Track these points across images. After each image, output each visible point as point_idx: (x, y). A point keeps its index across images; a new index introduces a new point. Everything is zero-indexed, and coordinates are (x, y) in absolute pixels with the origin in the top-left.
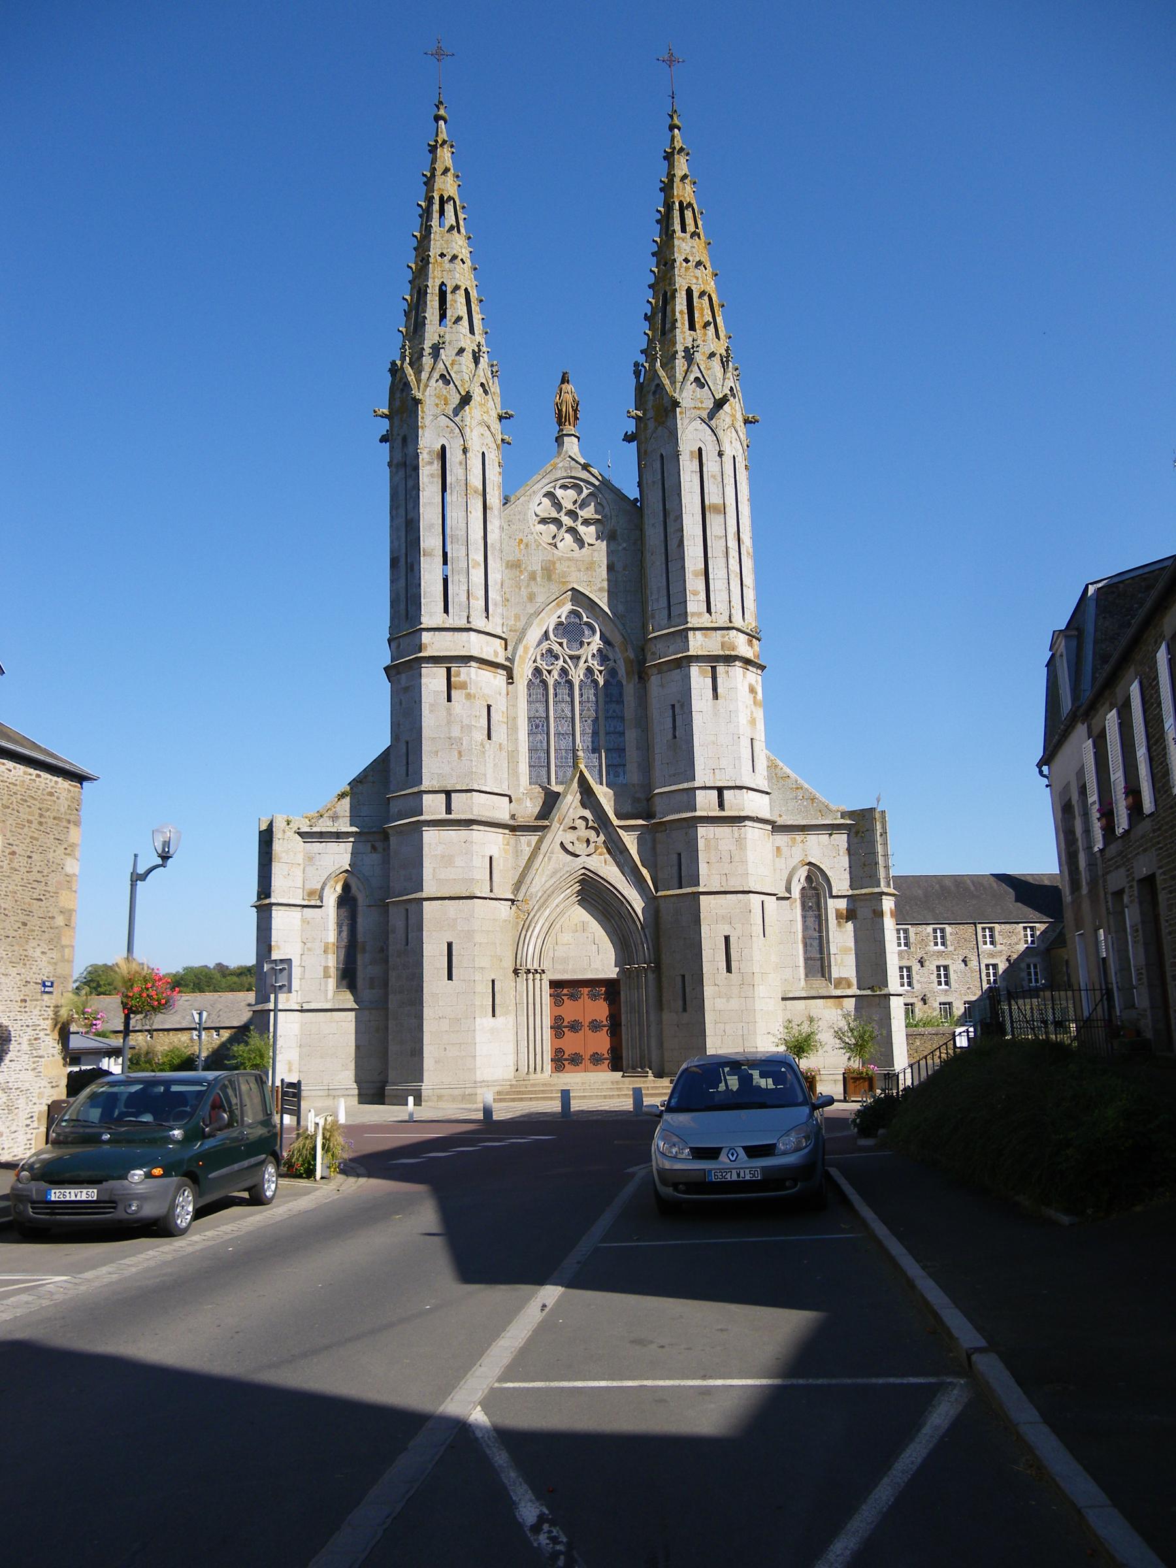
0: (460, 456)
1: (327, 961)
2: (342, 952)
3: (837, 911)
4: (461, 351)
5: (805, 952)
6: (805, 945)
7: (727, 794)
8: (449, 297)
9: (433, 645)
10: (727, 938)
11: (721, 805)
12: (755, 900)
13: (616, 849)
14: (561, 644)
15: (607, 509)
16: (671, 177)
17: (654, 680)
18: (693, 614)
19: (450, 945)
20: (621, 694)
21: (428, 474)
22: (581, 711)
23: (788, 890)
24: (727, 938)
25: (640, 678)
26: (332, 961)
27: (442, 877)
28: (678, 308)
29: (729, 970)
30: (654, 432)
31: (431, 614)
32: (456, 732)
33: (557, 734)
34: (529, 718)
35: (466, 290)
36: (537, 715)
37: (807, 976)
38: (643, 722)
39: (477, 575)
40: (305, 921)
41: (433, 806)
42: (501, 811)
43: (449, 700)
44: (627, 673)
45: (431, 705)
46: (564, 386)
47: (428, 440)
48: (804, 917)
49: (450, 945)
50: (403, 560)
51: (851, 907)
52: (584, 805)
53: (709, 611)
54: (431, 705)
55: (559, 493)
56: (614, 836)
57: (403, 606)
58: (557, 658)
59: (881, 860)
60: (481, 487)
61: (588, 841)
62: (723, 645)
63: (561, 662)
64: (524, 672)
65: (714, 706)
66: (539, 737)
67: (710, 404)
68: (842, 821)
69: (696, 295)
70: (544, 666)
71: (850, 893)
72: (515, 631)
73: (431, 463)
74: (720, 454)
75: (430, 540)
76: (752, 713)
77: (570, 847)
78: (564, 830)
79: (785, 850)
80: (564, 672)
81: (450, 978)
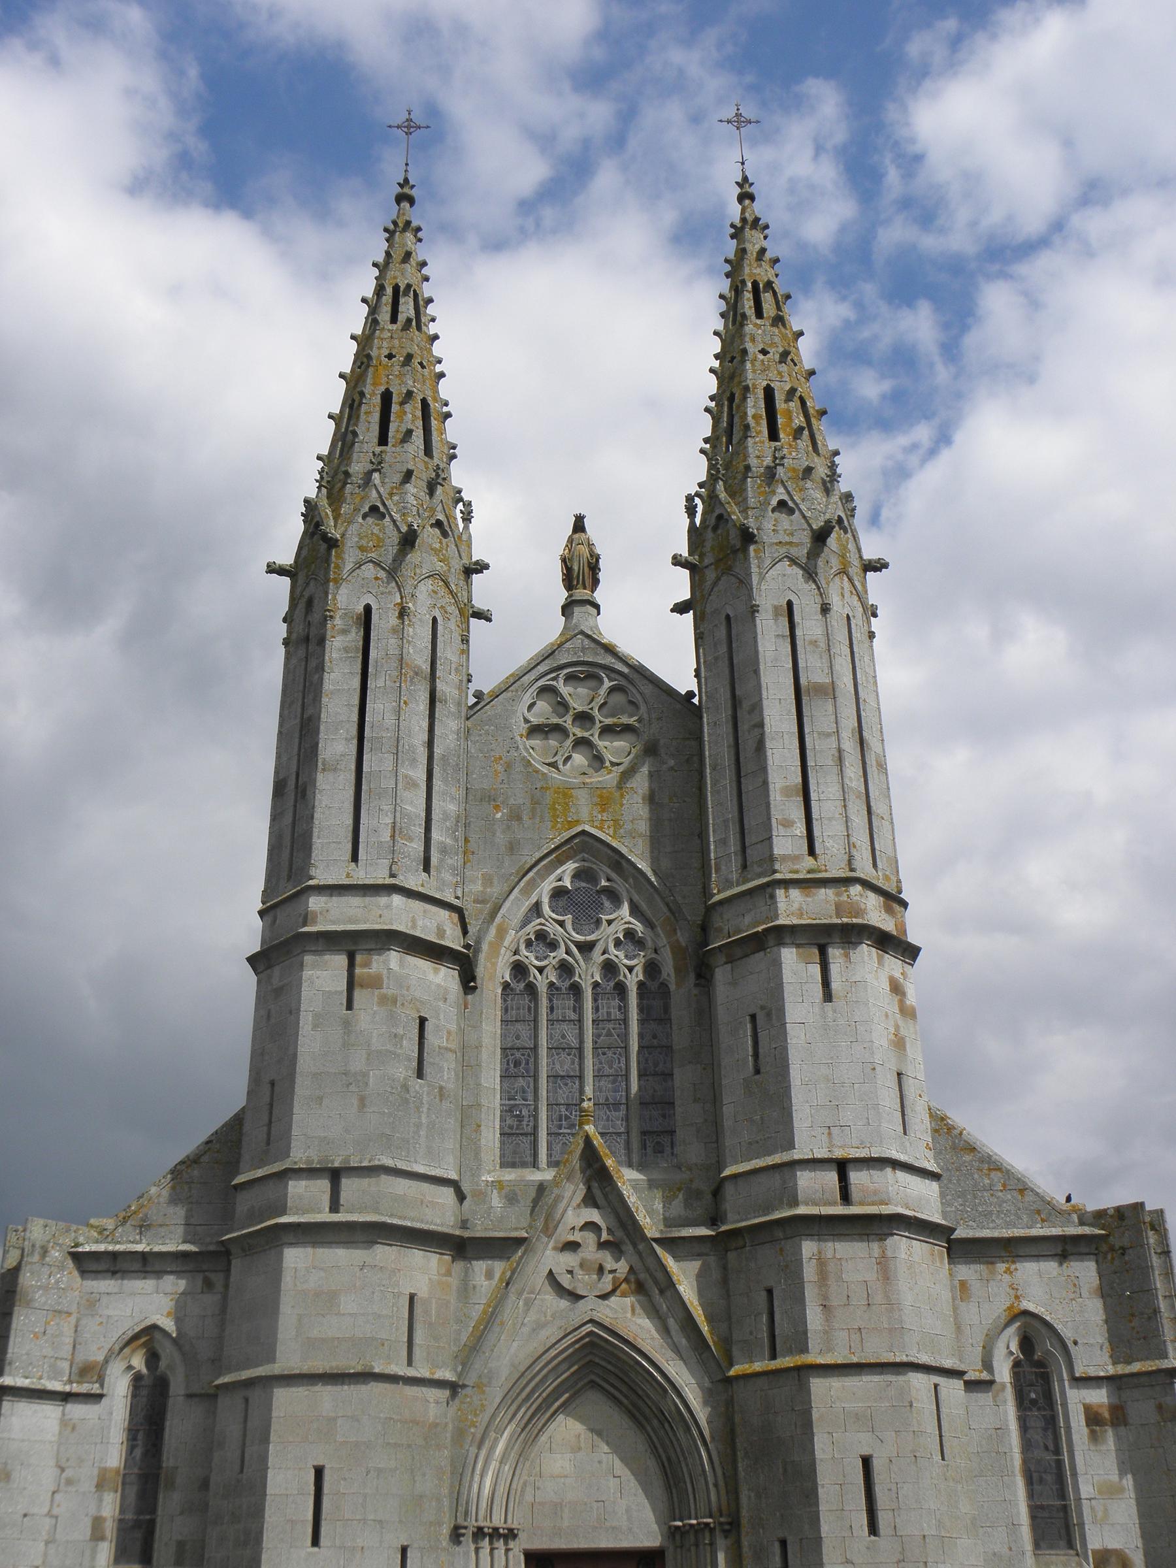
0: (393, 621)
1: (99, 1507)
2: (132, 1492)
3: (1088, 1409)
4: (408, 475)
5: (1031, 1495)
6: (1029, 1481)
7: (856, 1177)
8: (395, 408)
9: (330, 914)
10: (866, 1462)
11: (846, 1197)
12: (920, 1383)
13: (651, 1286)
14: (561, 924)
15: (643, 709)
16: (742, 252)
17: (721, 975)
18: (785, 858)
19: (319, 1472)
20: (666, 1009)
21: (340, 645)
22: (596, 1036)
23: (988, 1365)
24: (866, 1462)
25: (699, 976)
26: (110, 1506)
27: (315, 1333)
28: (750, 412)
29: (873, 1529)
30: (715, 584)
31: (328, 863)
32: (358, 1063)
33: (553, 1077)
34: (503, 1049)
35: (424, 402)
36: (518, 1043)
37: (1037, 1545)
38: (706, 1051)
39: (415, 804)
40: (65, 1423)
41: (307, 1200)
42: (438, 1211)
43: (350, 1006)
44: (678, 970)
45: (317, 1016)
46: (576, 536)
47: (346, 599)
48: (1024, 1427)
49: (319, 1472)
50: (291, 783)
51: (1116, 1401)
52: (589, 1200)
53: (812, 852)
54: (317, 1016)
55: (565, 690)
56: (650, 1261)
57: (286, 854)
58: (553, 946)
59: (1156, 1261)
60: (426, 667)
61: (601, 1270)
62: (839, 909)
63: (561, 953)
64: (494, 970)
65: (824, 1016)
66: (521, 1082)
67: (805, 538)
68: (1087, 1230)
69: (779, 397)
70: (530, 958)
71: (1111, 1370)
72: (483, 902)
73: (344, 632)
74: (825, 609)
75: (335, 744)
76: (897, 1027)
77: (565, 1280)
78: (555, 1249)
79: (975, 1286)
80: (565, 968)
81: (315, 1542)
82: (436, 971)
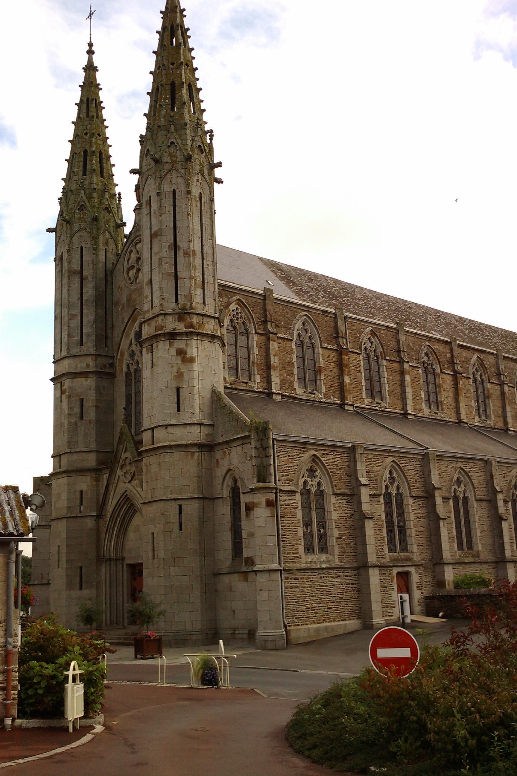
82: (86, 380)
